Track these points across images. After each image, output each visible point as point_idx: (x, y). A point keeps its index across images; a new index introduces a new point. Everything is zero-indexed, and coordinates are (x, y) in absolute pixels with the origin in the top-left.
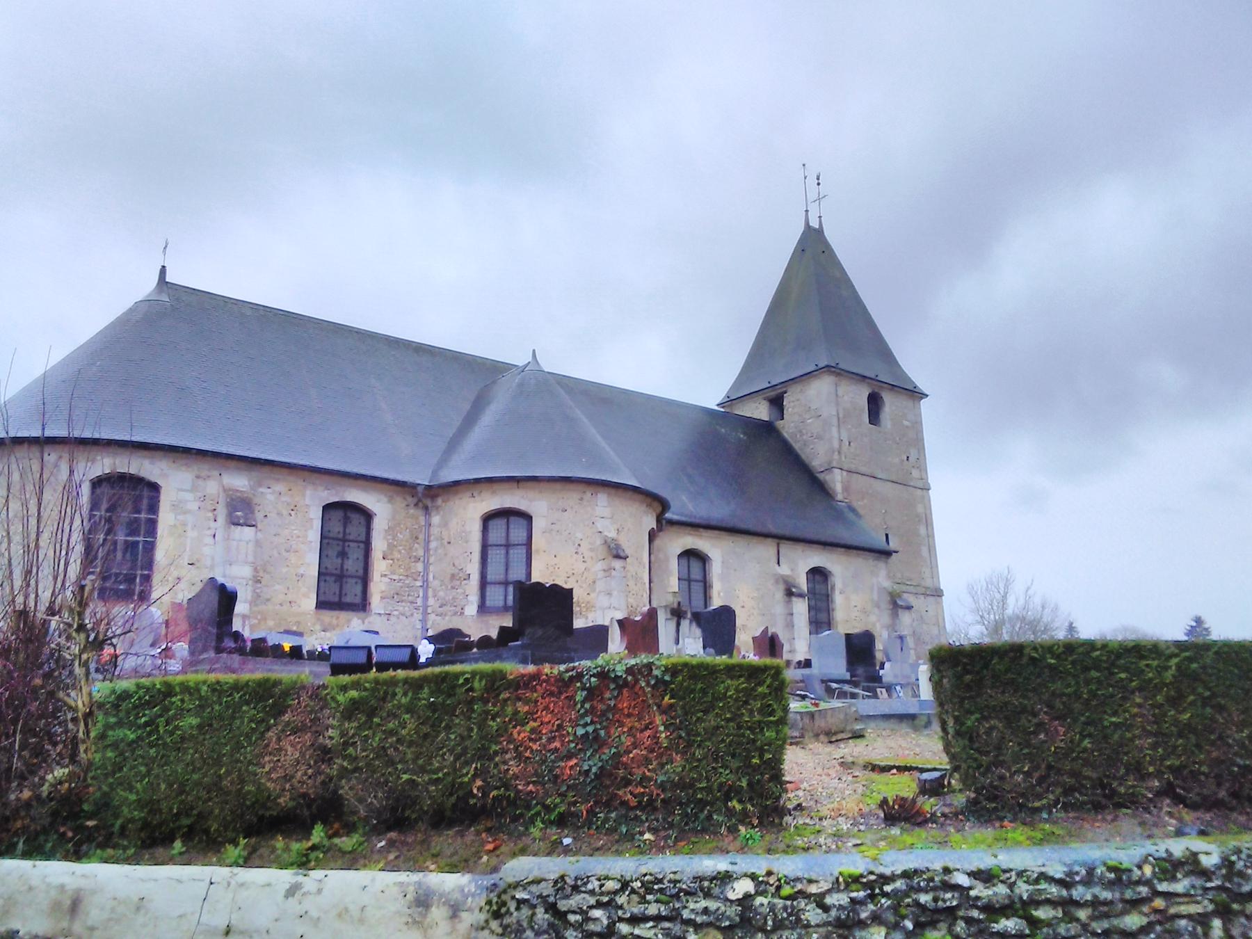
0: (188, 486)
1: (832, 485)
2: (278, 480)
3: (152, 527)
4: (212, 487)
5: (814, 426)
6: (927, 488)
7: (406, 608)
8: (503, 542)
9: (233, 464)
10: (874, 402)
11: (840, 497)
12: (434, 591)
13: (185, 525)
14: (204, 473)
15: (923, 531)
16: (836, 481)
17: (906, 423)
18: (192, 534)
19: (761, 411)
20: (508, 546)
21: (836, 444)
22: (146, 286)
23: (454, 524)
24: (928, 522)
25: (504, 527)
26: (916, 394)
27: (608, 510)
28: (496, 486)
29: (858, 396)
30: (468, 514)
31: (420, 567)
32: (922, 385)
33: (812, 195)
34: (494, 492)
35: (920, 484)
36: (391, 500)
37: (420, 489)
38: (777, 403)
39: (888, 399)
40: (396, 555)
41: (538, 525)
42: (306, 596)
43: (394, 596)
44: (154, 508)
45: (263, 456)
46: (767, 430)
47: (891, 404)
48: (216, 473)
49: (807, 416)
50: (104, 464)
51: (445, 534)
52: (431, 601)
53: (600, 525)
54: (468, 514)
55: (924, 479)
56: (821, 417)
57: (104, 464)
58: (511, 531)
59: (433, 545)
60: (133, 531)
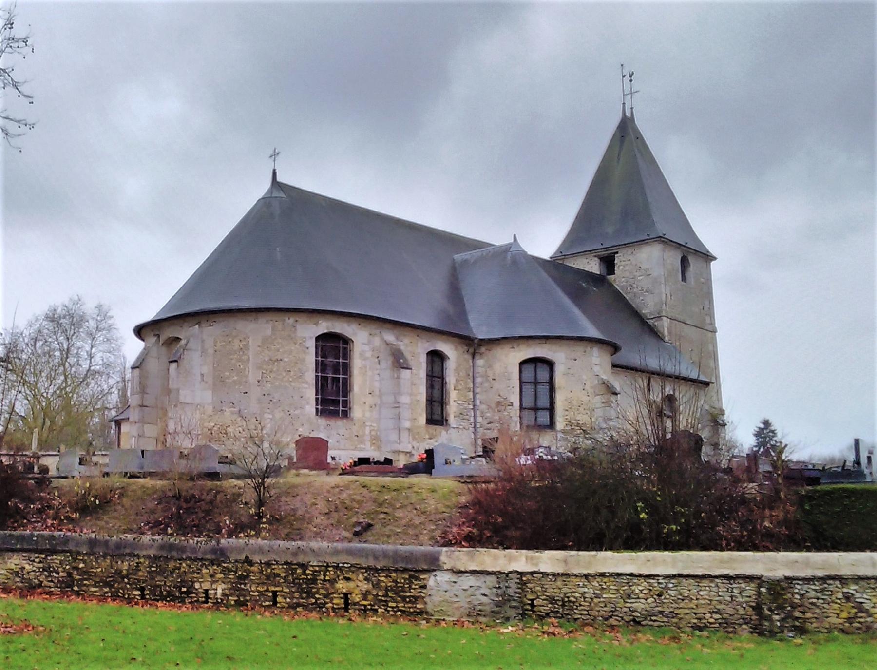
0: (366, 341)
1: (661, 329)
2: (405, 335)
3: (346, 368)
4: (377, 341)
5: (644, 282)
6: (714, 331)
7: (465, 424)
8: (533, 380)
9: (388, 325)
10: (684, 262)
11: (666, 339)
12: (482, 413)
13: (366, 367)
14: (373, 332)
15: (712, 364)
16: (664, 326)
17: (702, 280)
18: (369, 373)
19: (594, 266)
20: (536, 383)
21: (664, 299)
22: (263, 188)
23: (498, 367)
24: (715, 359)
25: (533, 370)
26: (708, 257)
27: (599, 359)
28: (531, 342)
29: (674, 258)
30: (510, 360)
31: (471, 395)
32: (713, 251)
33: (627, 91)
34: (365, 326)
35: (709, 328)
36: (456, 349)
37: (476, 341)
38: (609, 262)
39: (691, 259)
40: (460, 387)
41: (559, 370)
42: (421, 415)
43: (461, 415)
44: (346, 354)
45: (381, 316)
46: (599, 280)
47: (694, 264)
48: (378, 331)
49: (637, 274)
50: (324, 326)
51: (490, 373)
52: (479, 419)
53: (596, 369)
54: (510, 360)
55: (712, 323)
56: (644, 271)
57: (324, 326)
58: (538, 372)
59: (478, 380)
60: (336, 371)
